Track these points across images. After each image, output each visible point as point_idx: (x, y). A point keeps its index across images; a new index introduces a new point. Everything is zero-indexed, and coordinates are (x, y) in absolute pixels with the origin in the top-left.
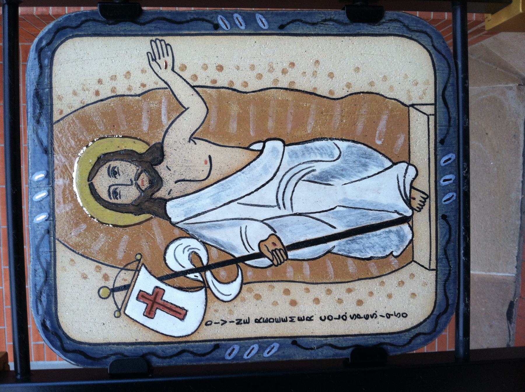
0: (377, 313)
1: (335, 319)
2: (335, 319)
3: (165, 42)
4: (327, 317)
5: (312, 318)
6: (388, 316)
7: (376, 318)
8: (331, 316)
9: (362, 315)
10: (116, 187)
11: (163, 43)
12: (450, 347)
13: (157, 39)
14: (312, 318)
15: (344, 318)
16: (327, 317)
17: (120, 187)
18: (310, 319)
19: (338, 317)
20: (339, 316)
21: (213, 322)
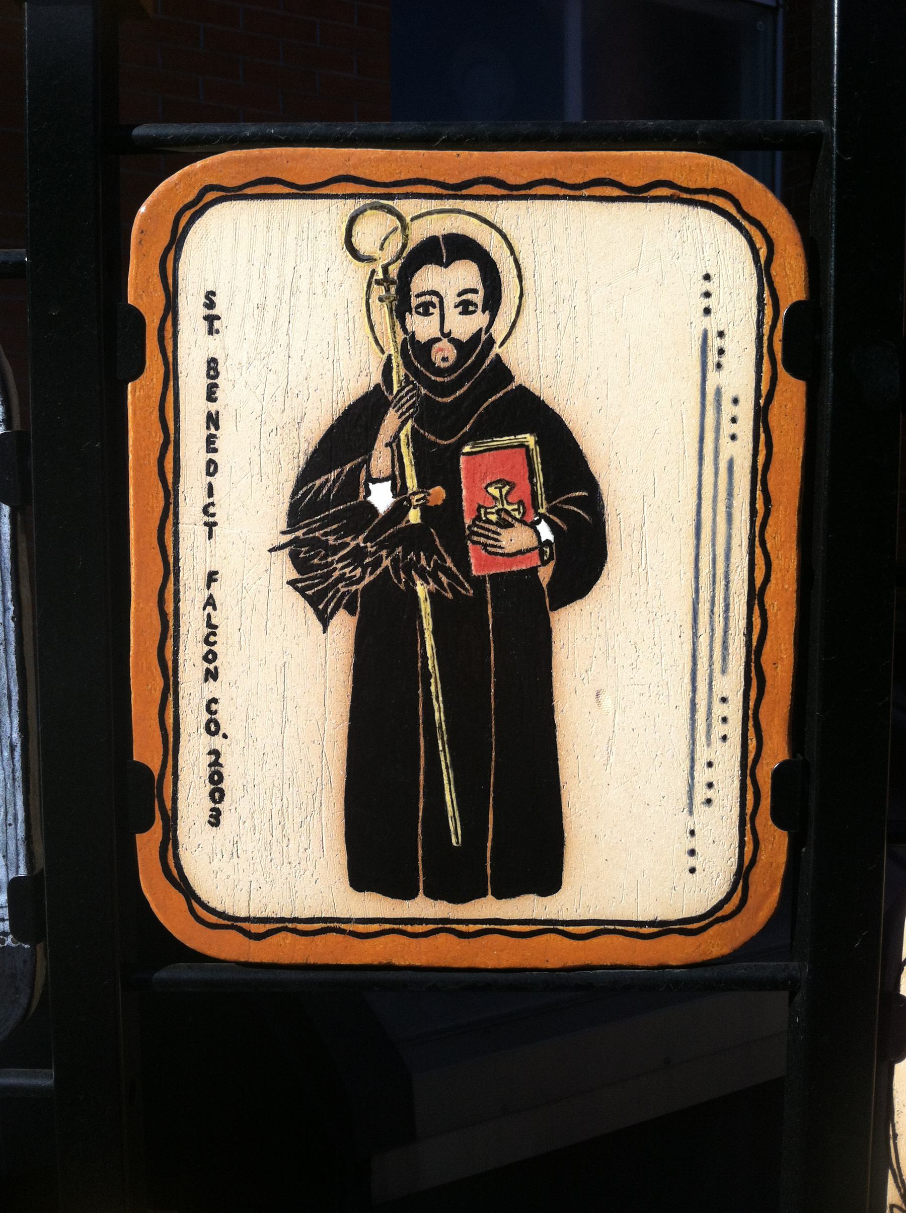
4: (212, 648)
6: (210, 657)
16: (212, 648)
18: (211, 675)
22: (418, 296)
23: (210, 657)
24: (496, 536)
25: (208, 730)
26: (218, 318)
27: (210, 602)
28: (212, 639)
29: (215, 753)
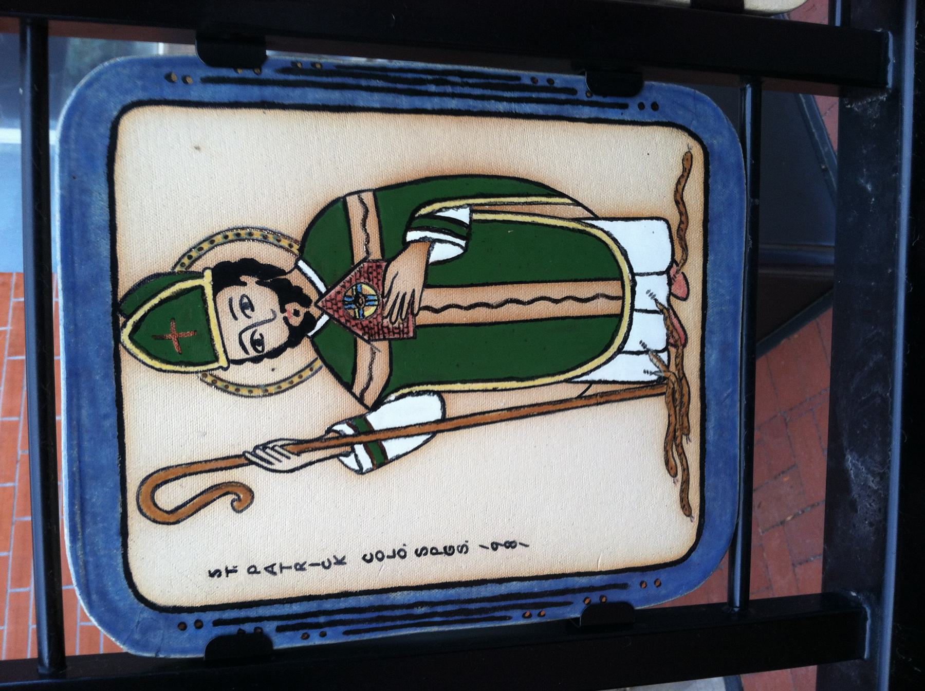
0: (467, 544)
1: (389, 557)
2: (389, 557)
3: (278, 446)
5: (345, 561)
6: (495, 546)
7: (466, 552)
8: (405, 553)
9: (441, 549)
10: (250, 332)
11: (277, 448)
12: (718, 596)
13: (275, 446)
14: (345, 561)
15: (400, 554)
17: (258, 328)
18: (464, 549)
19: (391, 554)
20: (394, 551)
21: (293, 568)
22: (246, 352)
23: (449, 551)
24: (407, 300)
25: (404, 557)
26: (226, 568)
27: (270, 569)
28: (327, 564)
29: (418, 554)
